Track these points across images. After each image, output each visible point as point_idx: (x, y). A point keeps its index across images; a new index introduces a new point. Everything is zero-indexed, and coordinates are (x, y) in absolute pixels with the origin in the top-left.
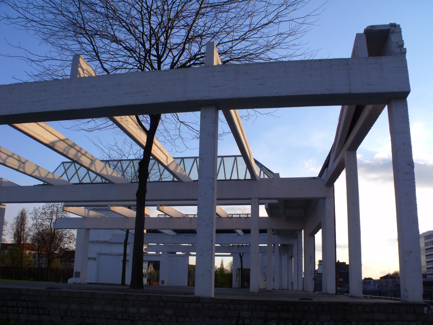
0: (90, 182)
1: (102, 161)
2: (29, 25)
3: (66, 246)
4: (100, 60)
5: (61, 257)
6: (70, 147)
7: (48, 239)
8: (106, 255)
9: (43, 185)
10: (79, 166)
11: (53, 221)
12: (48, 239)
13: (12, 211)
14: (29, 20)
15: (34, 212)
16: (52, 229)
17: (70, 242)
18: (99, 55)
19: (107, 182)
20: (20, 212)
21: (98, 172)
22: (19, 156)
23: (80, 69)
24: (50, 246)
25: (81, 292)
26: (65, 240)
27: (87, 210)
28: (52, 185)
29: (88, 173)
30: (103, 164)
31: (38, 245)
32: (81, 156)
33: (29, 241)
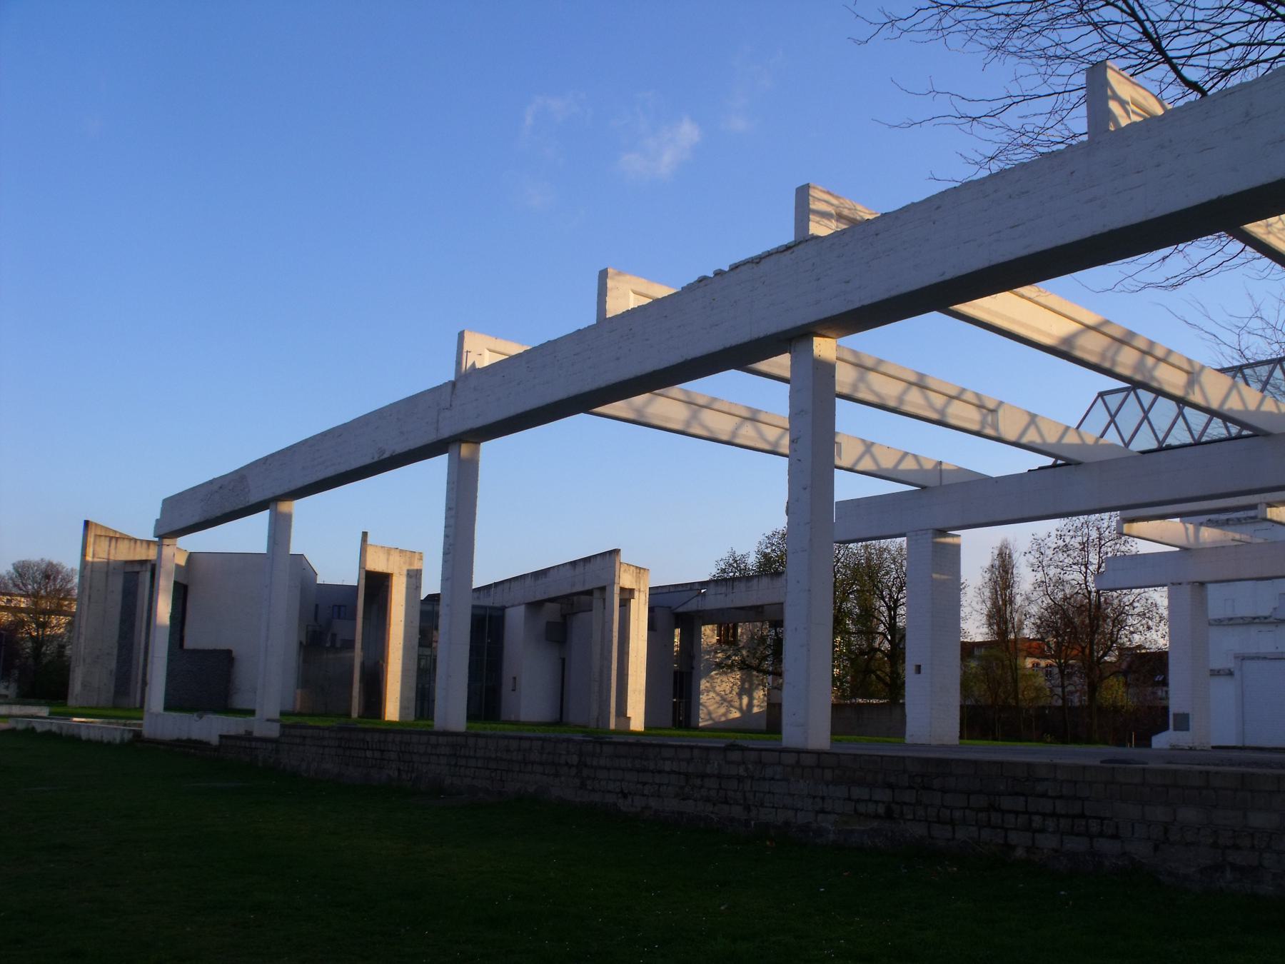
0: (1189, 440)
1: (1223, 371)
2: (947, 22)
3: (1137, 639)
4: (1168, 60)
5: (1125, 673)
6: (1117, 344)
7: (1083, 622)
8: (1265, 658)
9: (1054, 466)
10: (1151, 396)
11: (1092, 568)
12: (1082, 623)
13: (977, 549)
14: (945, 8)
15: (1035, 547)
16: (1090, 592)
17: (1149, 628)
18: (1164, 44)
19: (1245, 433)
20: (996, 552)
21: (1215, 405)
22: (977, 395)
23: (1114, 106)
24: (1091, 643)
25: (1208, 773)
26: (1130, 621)
27: (1191, 527)
28: (1078, 464)
29: (1181, 413)
30: (1226, 380)
31: (1057, 643)
32: (1155, 367)
33: (1028, 632)
